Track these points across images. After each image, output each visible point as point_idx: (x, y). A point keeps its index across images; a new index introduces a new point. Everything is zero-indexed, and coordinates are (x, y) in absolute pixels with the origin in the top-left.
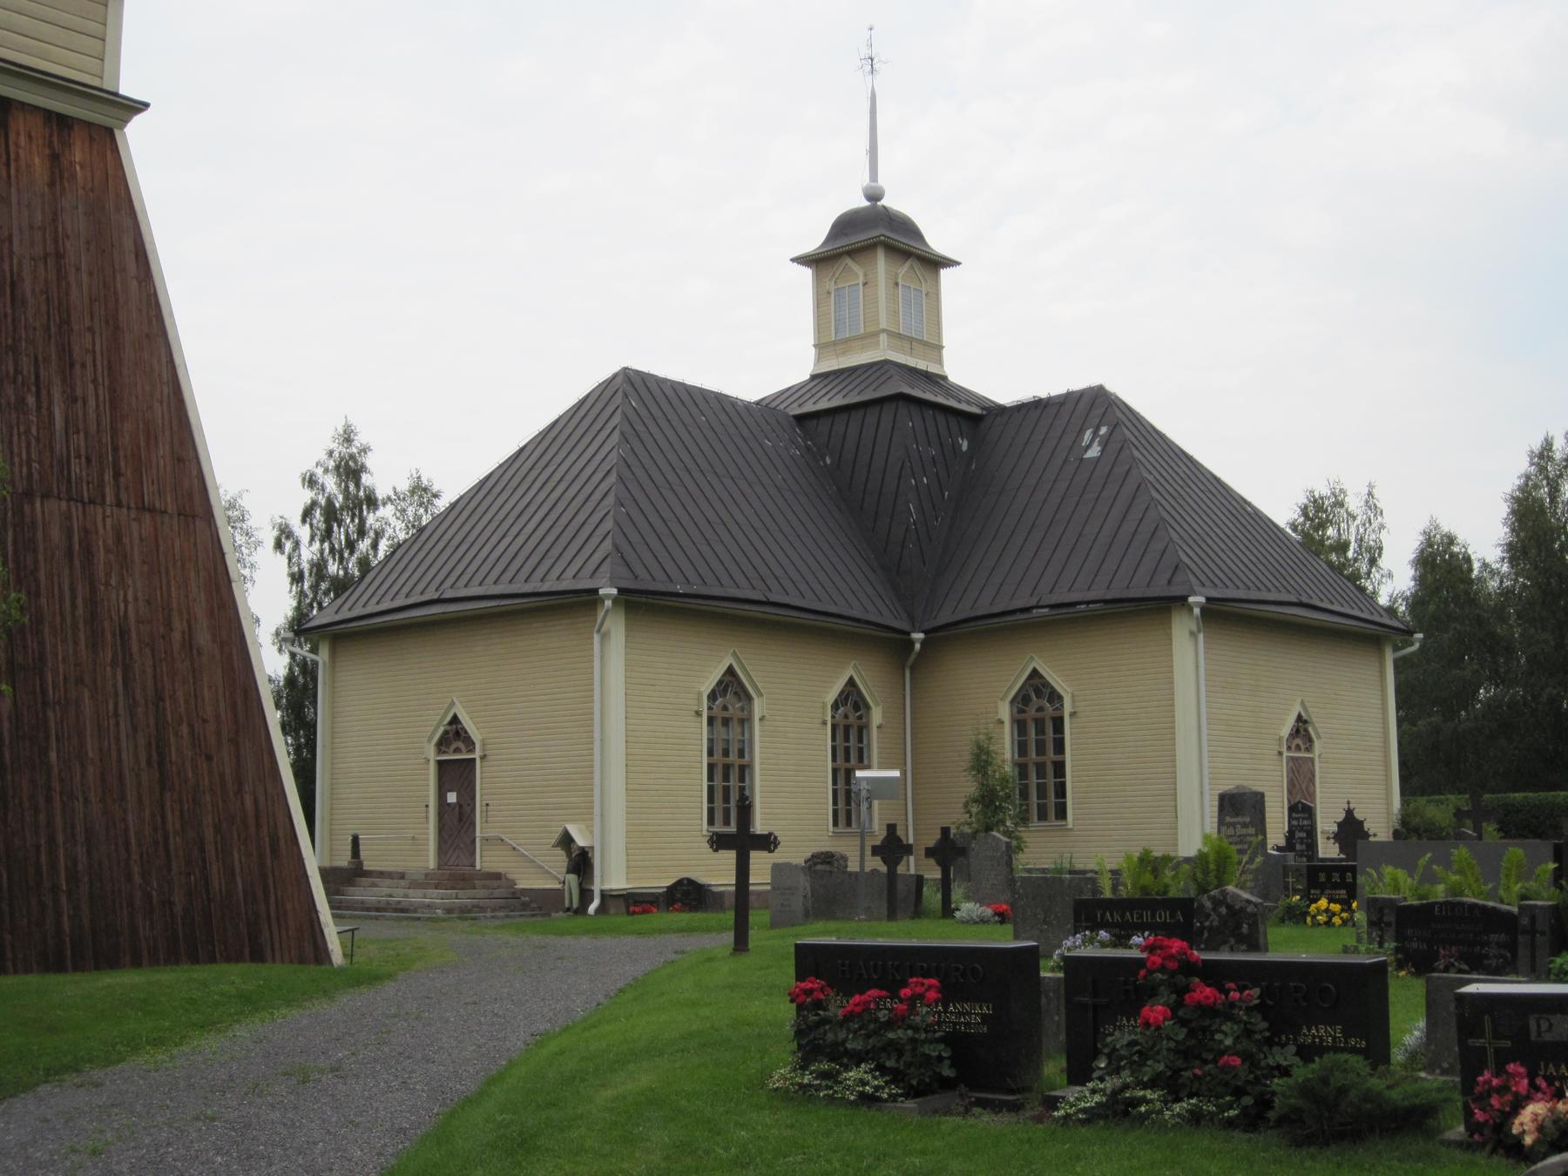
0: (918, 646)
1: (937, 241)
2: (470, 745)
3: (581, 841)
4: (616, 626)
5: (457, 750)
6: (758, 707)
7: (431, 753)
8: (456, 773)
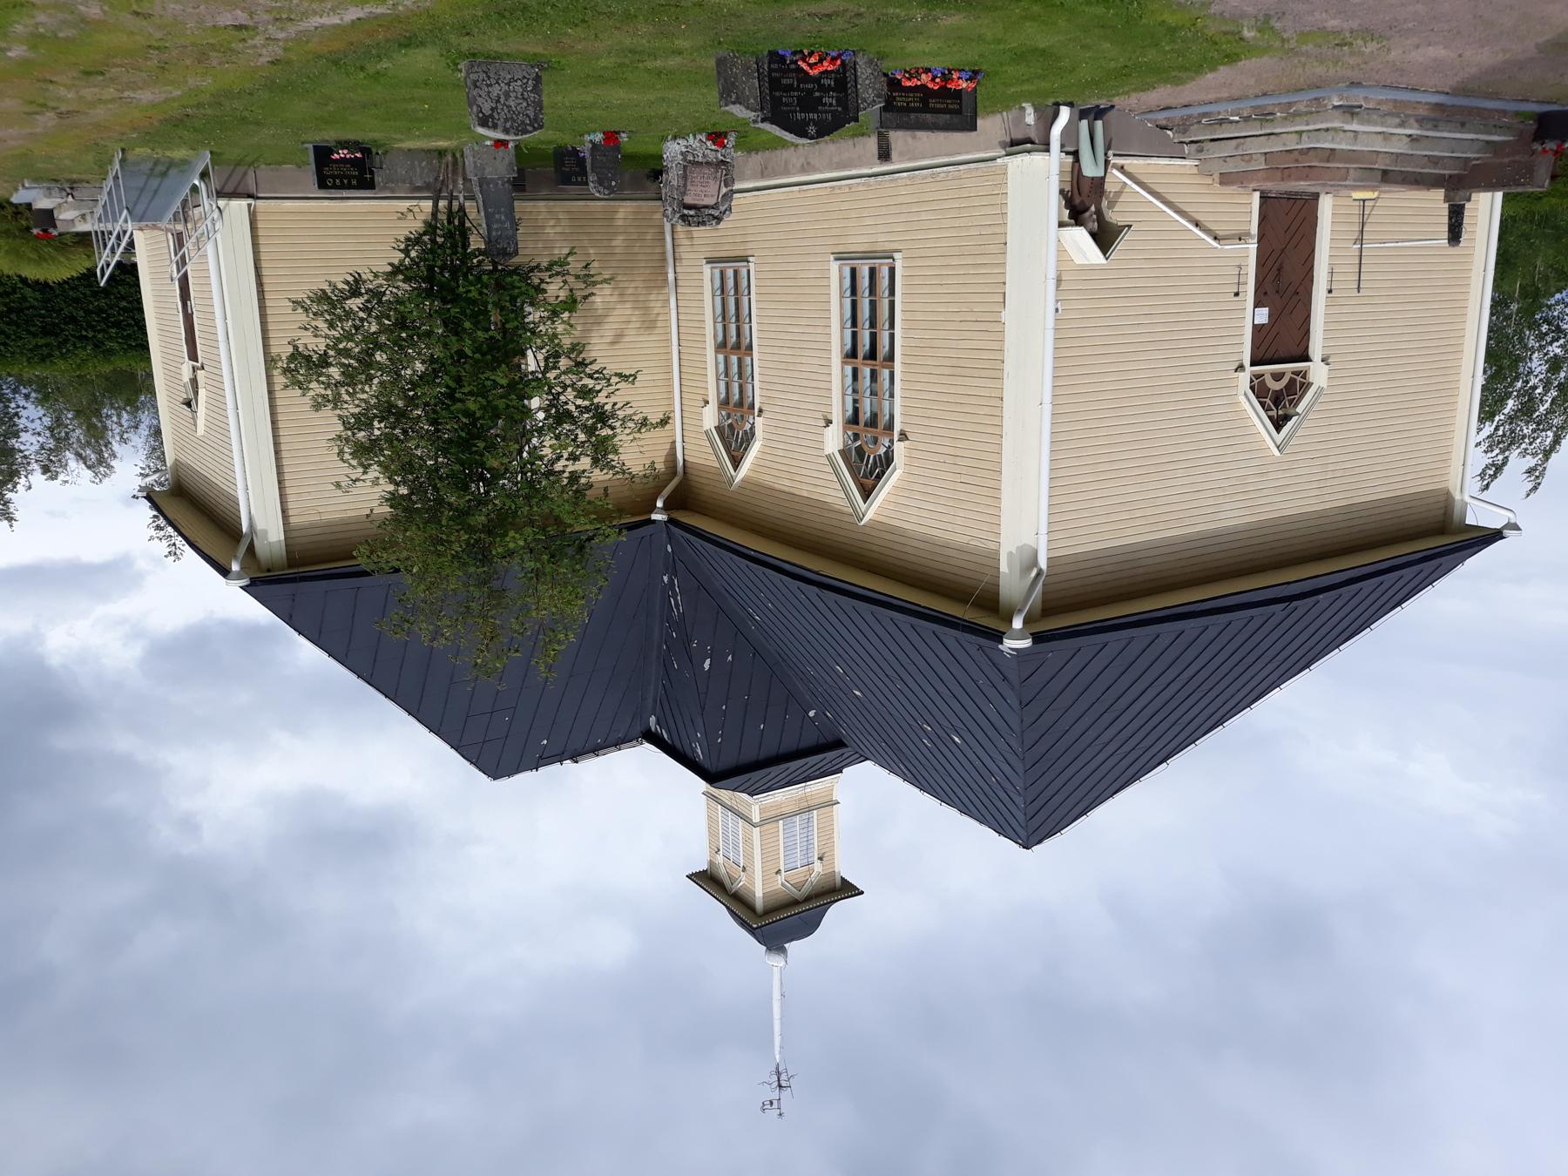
0: (659, 504)
2: (1259, 389)
3: (1080, 238)
4: (1012, 583)
5: (1277, 377)
6: (834, 439)
7: (1318, 373)
8: (1282, 343)
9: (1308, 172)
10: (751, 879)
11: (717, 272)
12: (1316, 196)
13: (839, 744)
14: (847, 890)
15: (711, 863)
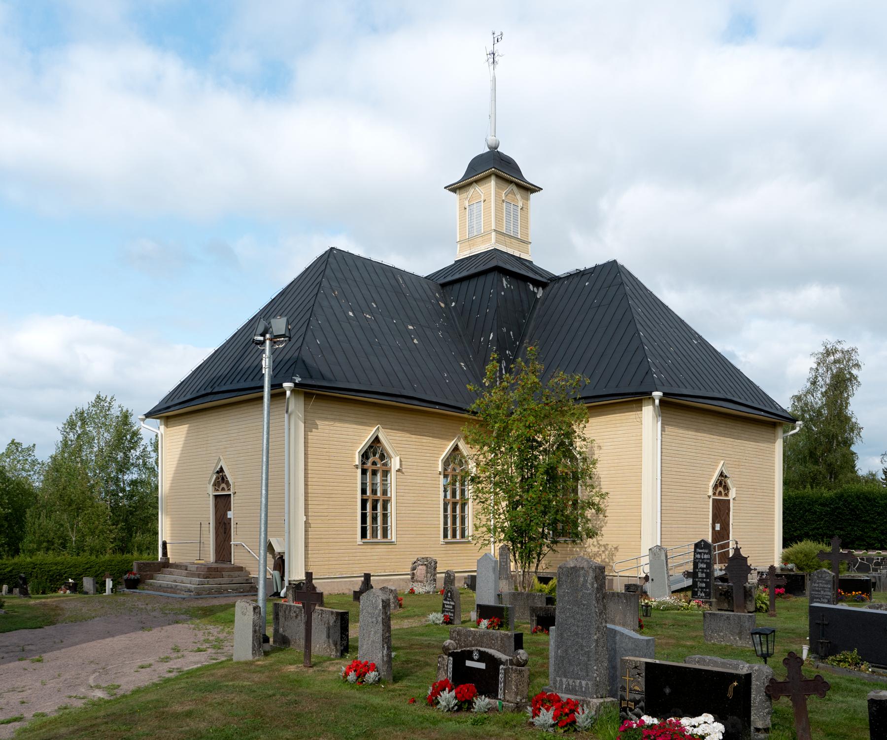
1: (530, 175)
2: (228, 483)
5: (223, 489)
8: (222, 503)
9: (216, 570)
10: (497, 195)
11: (389, 537)
12: (216, 562)
13: (443, 285)
14: (454, 189)
15: (527, 199)
